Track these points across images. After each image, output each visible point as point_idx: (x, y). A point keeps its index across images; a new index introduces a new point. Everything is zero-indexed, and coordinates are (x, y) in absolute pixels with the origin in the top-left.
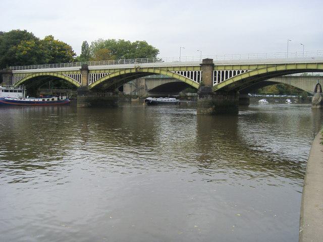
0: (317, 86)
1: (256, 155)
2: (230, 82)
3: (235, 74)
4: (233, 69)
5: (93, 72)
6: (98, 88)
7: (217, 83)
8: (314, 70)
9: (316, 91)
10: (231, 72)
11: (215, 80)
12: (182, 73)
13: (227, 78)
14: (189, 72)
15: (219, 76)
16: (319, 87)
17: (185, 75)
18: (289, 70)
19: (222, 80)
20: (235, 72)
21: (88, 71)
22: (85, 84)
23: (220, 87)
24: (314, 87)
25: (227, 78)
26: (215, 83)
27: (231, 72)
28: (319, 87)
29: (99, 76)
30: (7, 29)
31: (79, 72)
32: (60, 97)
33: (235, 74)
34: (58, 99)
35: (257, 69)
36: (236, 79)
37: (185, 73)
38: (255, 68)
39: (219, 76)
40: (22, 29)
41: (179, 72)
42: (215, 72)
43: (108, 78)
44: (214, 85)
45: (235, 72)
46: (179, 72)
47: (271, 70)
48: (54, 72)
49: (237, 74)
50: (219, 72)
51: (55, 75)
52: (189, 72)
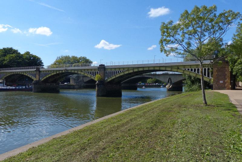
0: (169, 79)
1: (232, 53)
2: (114, 77)
3: (116, 73)
4: (115, 70)
5: (42, 72)
6: (46, 81)
7: (107, 78)
8: (157, 70)
9: (169, 82)
10: (114, 72)
11: (106, 76)
12: (192, 70)
13: (112, 75)
14: (92, 72)
15: (108, 74)
16: (170, 80)
17: (90, 74)
18: (151, 70)
19: (110, 76)
20: (116, 72)
21: (40, 71)
22: (38, 79)
23: (109, 80)
24: (168, 80)
25: (112, 75)
26: (106, 78)
27: (114, 72)
28: (170, 80)
29: (46, 75)
30: (2, 48)
31: (35, 72)
32: (27, 86)
33: (116, 73)
34: (26, 87)
35: (128, 70)
36: (117, 76)
37: (90, 72)
38: (127, 69)
39: (108, 74)
40: (10, 47)
41: (87, 72)
42: (106, 72)
43: (50, 75)
44: (105, 79)
45: (116, 72)
46: (87, 72)
47: (136, 70)
48: (22, 72)
49: (117, 73)
50: (108, 72)
51: (22, 73)
52: (92, 72)
